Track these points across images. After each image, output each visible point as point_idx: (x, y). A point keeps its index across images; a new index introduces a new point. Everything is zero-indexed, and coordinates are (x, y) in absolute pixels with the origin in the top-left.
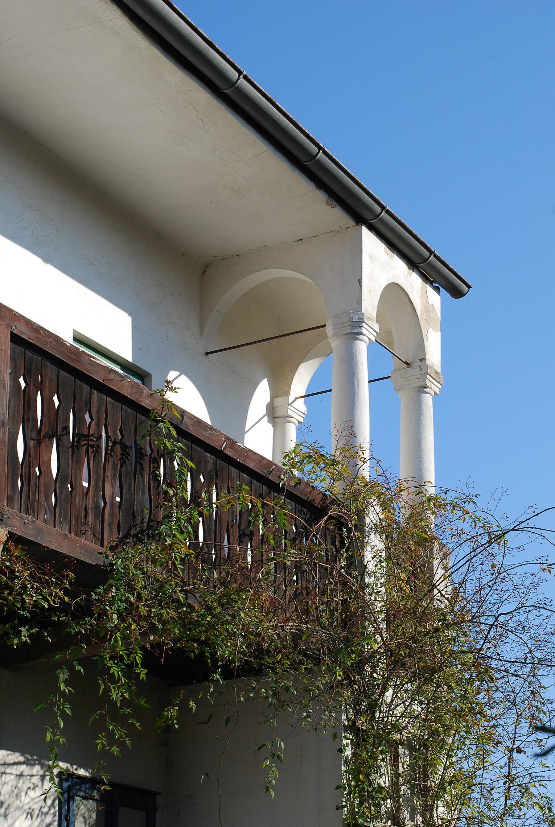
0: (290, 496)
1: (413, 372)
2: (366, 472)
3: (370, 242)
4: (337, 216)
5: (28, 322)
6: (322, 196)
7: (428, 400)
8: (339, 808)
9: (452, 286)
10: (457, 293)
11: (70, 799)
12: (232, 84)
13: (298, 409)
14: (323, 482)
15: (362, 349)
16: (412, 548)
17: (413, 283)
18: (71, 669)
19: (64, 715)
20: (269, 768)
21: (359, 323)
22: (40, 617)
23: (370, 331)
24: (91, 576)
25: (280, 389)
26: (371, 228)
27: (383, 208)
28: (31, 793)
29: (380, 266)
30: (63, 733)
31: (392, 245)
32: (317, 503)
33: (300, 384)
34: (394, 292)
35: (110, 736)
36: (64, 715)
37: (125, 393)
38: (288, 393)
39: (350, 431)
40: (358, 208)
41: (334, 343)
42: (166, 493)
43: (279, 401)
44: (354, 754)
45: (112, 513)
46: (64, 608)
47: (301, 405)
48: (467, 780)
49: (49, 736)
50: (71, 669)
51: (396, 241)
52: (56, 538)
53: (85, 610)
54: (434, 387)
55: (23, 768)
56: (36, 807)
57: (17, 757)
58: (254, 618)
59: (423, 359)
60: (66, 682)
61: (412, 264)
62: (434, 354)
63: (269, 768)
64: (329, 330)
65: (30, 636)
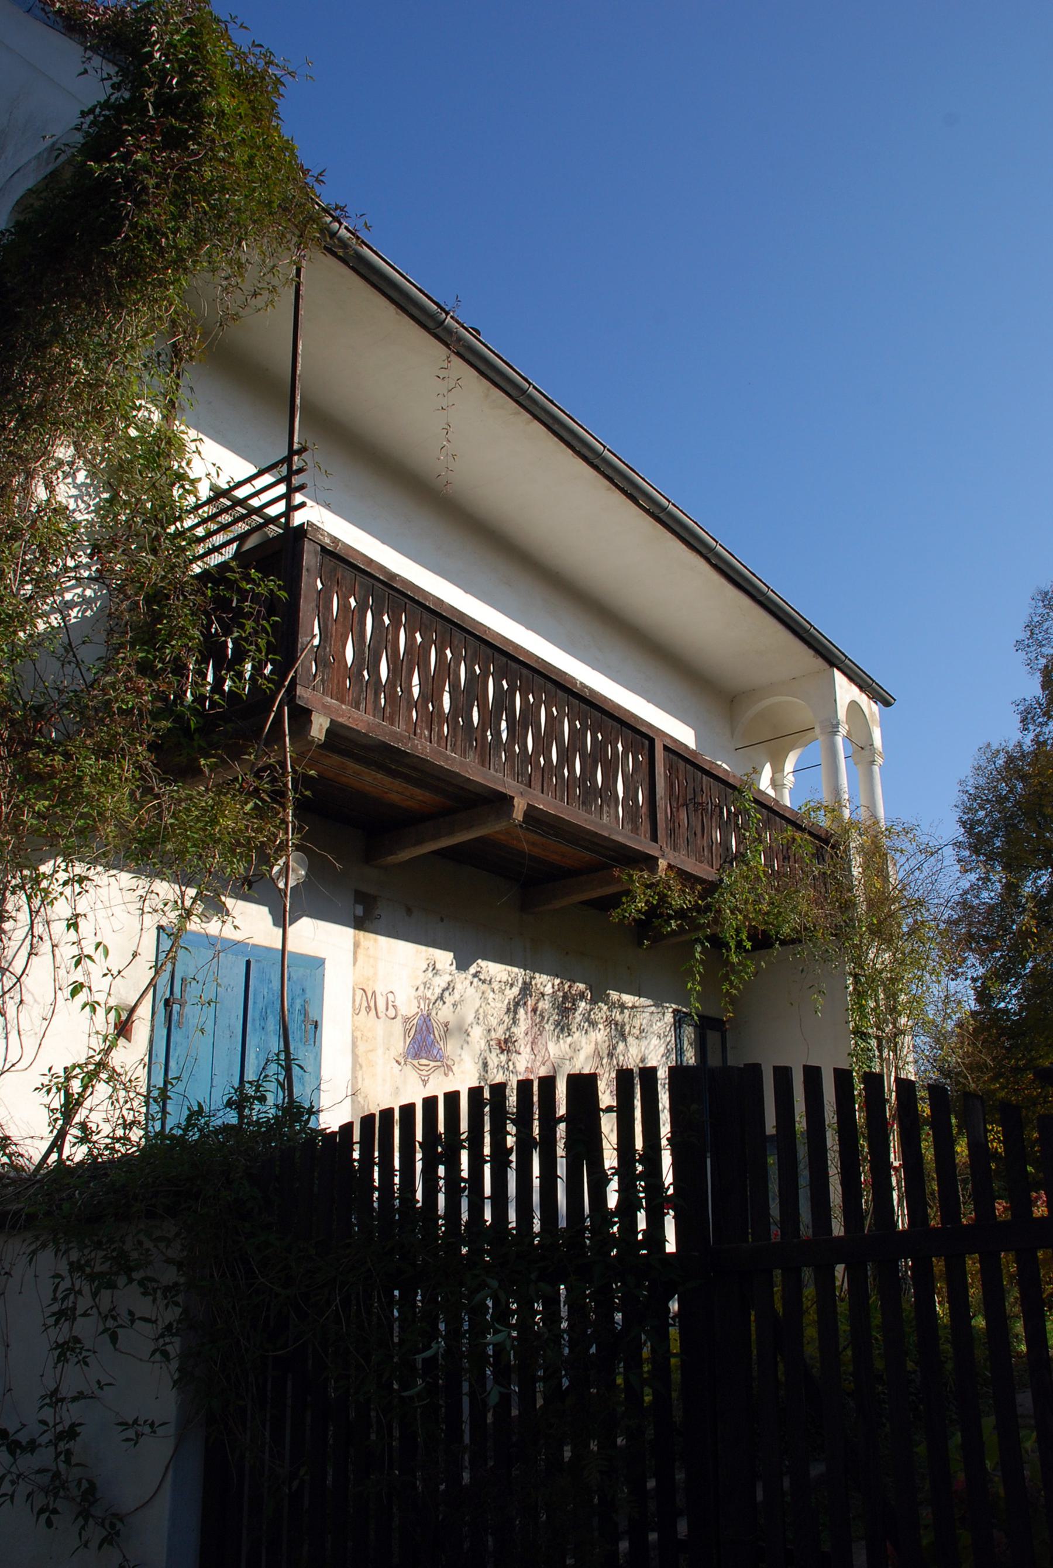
0: (811, 834)
1: (866, 753)
2: (847, 813)
3: (839, 677)
4: (820, 663)
5: (671, 737)
6: (811, 652)
7: (876, 769)
8: (847, 1022)
9: (884, 700)
10: (887, 703)
11: (680, 1027)
12: (764, 594)
13: (789, 780)
14: (823, 821)
15: (839, 740)
16: (876, 856)
17: (863, 699)
18: (703, 944)
19: (699, 972)
20: (817, 999)
21: (838, 724)
22: (681, 914)
23: (843, 730)
24: (711, 888)
25: (778, 769)
26: (839, 669)
27: (846, 657)
28: (658, 1024)
29: (845, 691)
30: (699, 984)
31: (851, 679)
32: (823, 836)
33: (789, 766)
34: (854, 705)
35: (731, 983)
36: (699, 972)
37: (720, 775)
38: (783, 770)
39: (836, 791)
40: (830, 657)
41: (821, 738)
42: (744, 835)
43: (777, 775)
44: (854, 989)
45: (717, 849)
46: (697, 908)
47: (791, 777)
48: (916, 999)
49: (689, 985)
50: (703, 944)
51: (853, 676)
52: (691, 866)
53: (708, 908)
54: (879, 761)
55: (653, 1008)
56: (661, 1032)
57: (650, 1002)
58: (804, 909)
59: (872, 745)
60: (700, 953)
61: (861, 688)
62: (878, 742)
63: (817, 999)
64: (817, 730)
65: (677, 926)
